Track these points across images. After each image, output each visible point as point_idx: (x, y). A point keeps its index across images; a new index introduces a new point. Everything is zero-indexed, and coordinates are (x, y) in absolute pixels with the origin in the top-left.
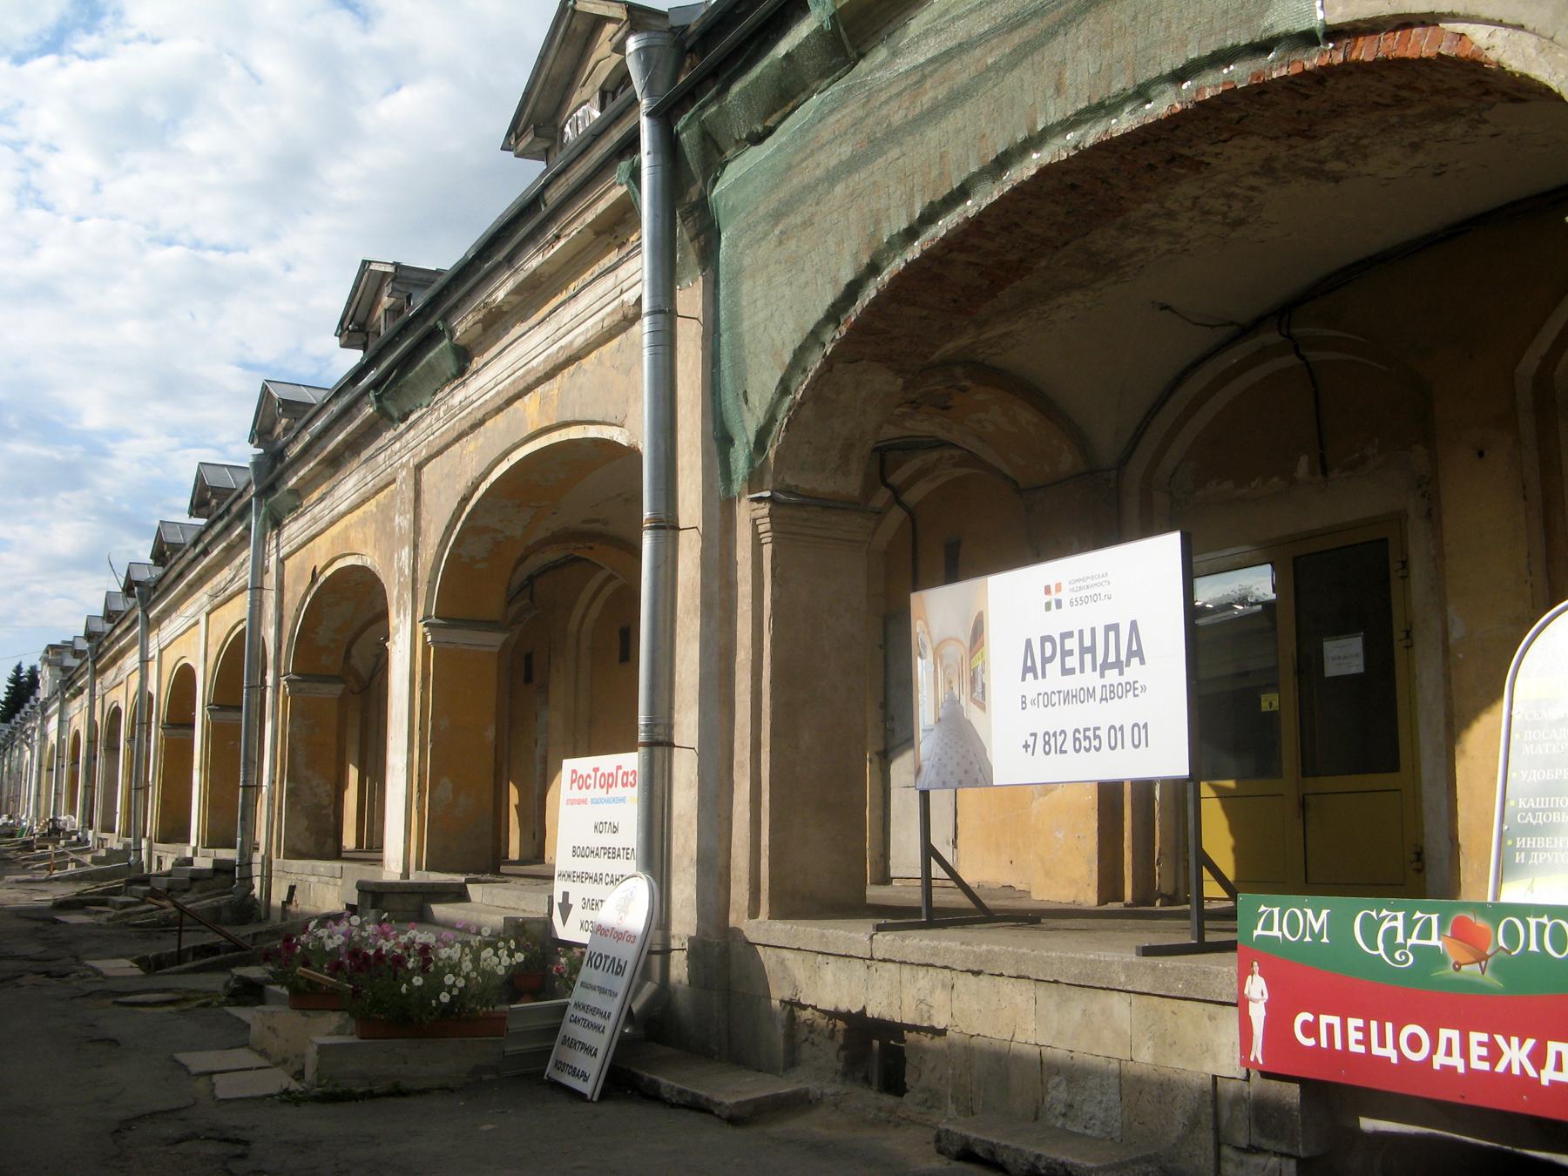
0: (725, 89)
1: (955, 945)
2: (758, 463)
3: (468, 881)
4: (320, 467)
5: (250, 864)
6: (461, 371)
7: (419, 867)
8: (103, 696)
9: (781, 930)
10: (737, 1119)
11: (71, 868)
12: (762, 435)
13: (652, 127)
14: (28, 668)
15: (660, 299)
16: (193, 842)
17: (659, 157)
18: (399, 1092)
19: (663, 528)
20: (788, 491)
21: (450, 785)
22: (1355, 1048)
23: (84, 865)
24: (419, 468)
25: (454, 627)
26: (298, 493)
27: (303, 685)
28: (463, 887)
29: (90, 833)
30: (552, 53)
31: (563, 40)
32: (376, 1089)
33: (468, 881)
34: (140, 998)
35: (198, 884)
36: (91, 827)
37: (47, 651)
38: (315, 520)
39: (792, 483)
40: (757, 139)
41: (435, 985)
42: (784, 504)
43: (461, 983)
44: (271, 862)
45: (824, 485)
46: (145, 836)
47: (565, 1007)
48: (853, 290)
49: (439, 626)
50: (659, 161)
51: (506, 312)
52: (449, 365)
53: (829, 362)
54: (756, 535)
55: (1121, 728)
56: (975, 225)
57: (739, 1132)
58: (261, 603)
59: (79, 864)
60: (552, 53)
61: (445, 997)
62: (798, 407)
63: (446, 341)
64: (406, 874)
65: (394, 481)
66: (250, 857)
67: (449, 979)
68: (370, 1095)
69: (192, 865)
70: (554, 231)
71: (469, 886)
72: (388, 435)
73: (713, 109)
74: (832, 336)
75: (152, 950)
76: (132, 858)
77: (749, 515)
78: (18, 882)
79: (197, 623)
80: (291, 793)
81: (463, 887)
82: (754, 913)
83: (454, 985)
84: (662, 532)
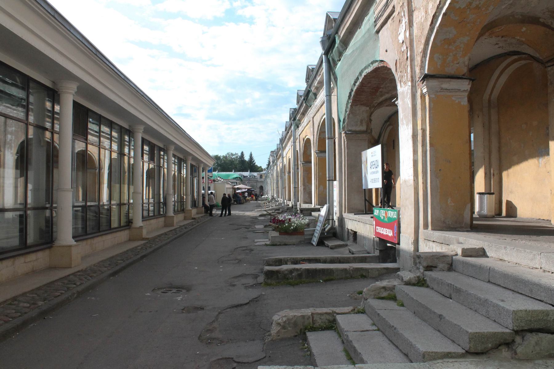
0: (332, 51)
1: (357, 217)
2: (344, 125)
3: (321, 207)
4: (302, 115)
5: (297, 205)
6: (316, 98)
7: (317, 205)
8: (279, 165)
9: (352, 216)
10: (332, 248)
11: (271, 208)
12: (344, 120)
13: (325, 57)
14: (75, 242)
15: (328, 93)
16: (292, 201)
17: (326, 63)
18: (285, 245)
19: (329, 139)
20: (350, 131)
21: (323, 187)
22: (390, 230)
23: (273, 207)
24: (313, 118)
25: (321, 153)
26: (300, 120)
27: (306, 164)
28: (319, 209)
29: (279, 199)
30: (327, 25)
31: (328, 22)
32: (281, 244)
33: (321, 207)
34: (257, 231)
35: (288, 210)
36: (279, 198)
37: (271, 153)
38: (302, 127)
39: (351, 129)
40: (340, 60)
41: (290, 225)
42: (348, 134)
43: (295, 225)
44: (301, 205)
45: (358, 128)
46: (285, 199)
47: (315, 230)
48: (350, 93)
49: (319, 153)
50: (326, 64)
51: (319, 87)
52: (314, 97)
53: (351, 106)
54: (344, 140)
55: (378, 178)
56: (362, 83)
57: (332, 250)
58: (296, 145)
59: (272, 206)
60: (327, 25)
61: (292, 228)
62: (349, 114)
63: (311, 93)
64: (315, 206)
65: (310, 121)
66: (297, 203)
67: (293, 224)
68: (280, 245)
69: (289, 206)
70: (319, 73)
71: (321, 208)
72: (309, 110)
73: (332, 55)
74: (351, 101)
75: (265, 224)
76: (283, 205)
77: (343, 135)
78: (257, 211)
79: (290, 149)
80: (304, 189)
81: (319, 209)
82: (345, 212)
83: (294, 225)
84: (329, 140)
